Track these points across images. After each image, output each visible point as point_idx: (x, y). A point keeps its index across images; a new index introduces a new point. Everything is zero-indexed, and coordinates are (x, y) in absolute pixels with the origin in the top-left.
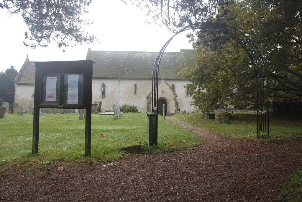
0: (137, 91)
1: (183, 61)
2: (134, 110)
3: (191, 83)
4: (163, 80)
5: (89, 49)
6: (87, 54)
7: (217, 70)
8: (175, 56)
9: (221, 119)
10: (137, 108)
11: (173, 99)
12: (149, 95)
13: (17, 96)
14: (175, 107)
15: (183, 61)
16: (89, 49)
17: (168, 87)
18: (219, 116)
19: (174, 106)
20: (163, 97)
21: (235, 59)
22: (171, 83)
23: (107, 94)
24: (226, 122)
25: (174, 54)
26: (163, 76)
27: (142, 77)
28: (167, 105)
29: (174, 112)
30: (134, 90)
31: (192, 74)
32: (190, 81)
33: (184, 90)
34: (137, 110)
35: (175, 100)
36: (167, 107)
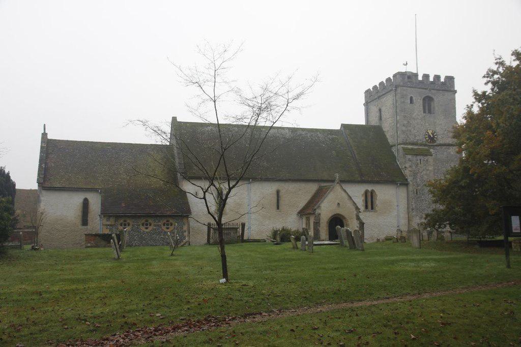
0: (281, 202)
5: (174, 119)
8: (334, 136)
11: (355, 216)
13: (42, 213)
16: (174, 119)
30: (275, 201)
33: (361, 201)
35: (358, 218)
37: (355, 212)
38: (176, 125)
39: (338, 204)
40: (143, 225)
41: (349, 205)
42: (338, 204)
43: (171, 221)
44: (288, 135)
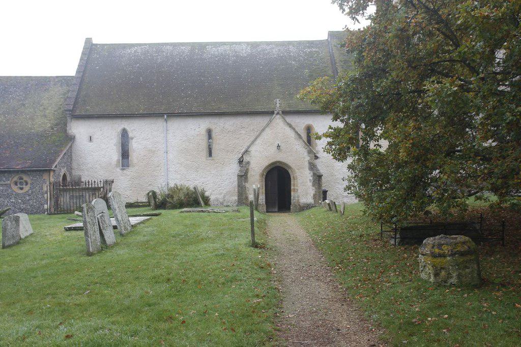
1: (333, 63)
2: (194, 200)
3: (339, 124)
4: (278, 116)
6: (83, 54)
7: (423, 77)
9: (442, 268)
10: (207, 194)
11: (307, 164)
12: (242, 157)
14: (313, 185)
15: (336, 63)
17: (292, 134)
18: (434, 255)
19: (311, 184)
20: (279, 162)
21: (501, 20)
22: (301, 122)
23: (134, 157)
24: (464, 279)
25: (311, 44)
26: (278, 105)
27: (224, 108)
28: (292, 183)
29: (310, 200)
31: (341, 96)
32: (335, 119)
34: (207, 201)
35: (312, 167)
36: (292, 188)
37: (308, 158)
38: (90, 49)
39: (278, 146)
40: (16, 184)
41: (297, 147)
42: (278, 146)
43: (25, 178)
44: (186, 49)
